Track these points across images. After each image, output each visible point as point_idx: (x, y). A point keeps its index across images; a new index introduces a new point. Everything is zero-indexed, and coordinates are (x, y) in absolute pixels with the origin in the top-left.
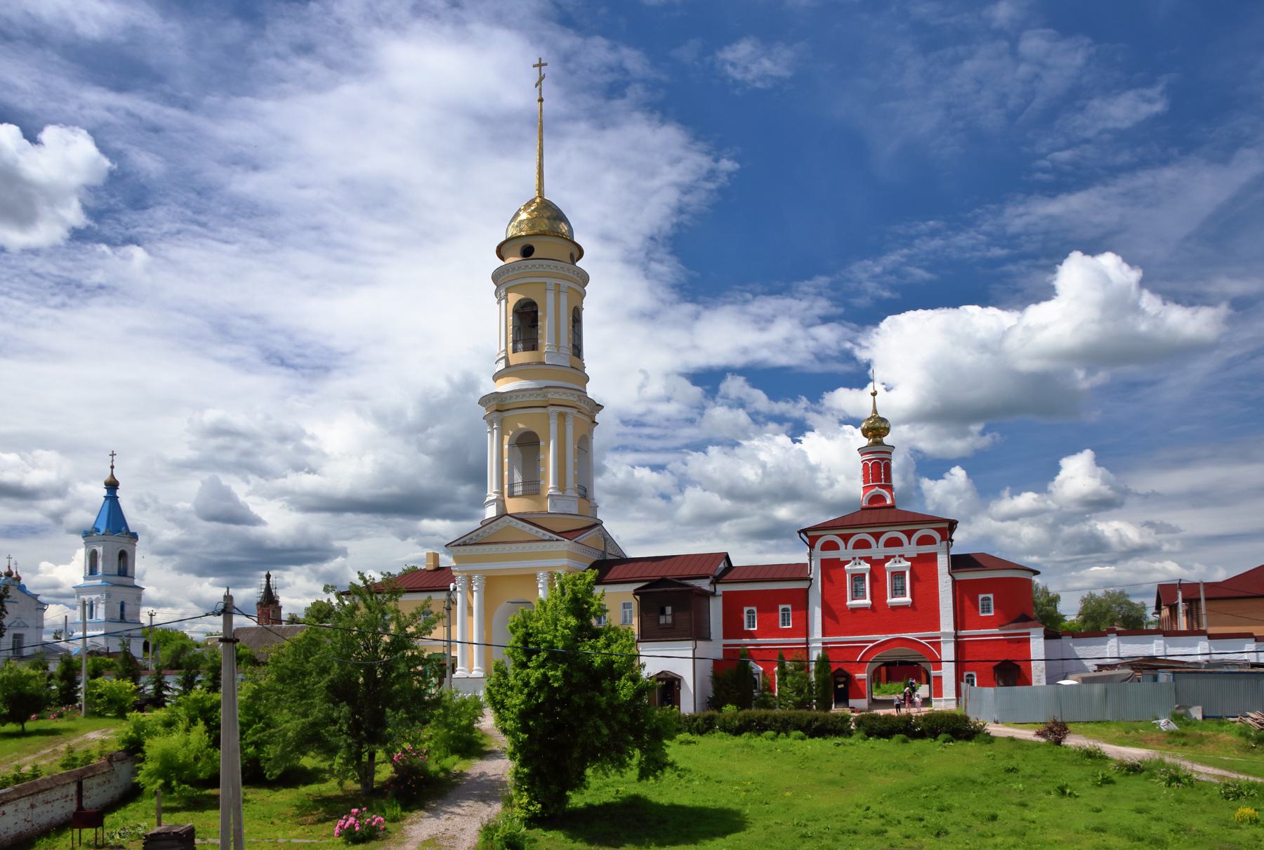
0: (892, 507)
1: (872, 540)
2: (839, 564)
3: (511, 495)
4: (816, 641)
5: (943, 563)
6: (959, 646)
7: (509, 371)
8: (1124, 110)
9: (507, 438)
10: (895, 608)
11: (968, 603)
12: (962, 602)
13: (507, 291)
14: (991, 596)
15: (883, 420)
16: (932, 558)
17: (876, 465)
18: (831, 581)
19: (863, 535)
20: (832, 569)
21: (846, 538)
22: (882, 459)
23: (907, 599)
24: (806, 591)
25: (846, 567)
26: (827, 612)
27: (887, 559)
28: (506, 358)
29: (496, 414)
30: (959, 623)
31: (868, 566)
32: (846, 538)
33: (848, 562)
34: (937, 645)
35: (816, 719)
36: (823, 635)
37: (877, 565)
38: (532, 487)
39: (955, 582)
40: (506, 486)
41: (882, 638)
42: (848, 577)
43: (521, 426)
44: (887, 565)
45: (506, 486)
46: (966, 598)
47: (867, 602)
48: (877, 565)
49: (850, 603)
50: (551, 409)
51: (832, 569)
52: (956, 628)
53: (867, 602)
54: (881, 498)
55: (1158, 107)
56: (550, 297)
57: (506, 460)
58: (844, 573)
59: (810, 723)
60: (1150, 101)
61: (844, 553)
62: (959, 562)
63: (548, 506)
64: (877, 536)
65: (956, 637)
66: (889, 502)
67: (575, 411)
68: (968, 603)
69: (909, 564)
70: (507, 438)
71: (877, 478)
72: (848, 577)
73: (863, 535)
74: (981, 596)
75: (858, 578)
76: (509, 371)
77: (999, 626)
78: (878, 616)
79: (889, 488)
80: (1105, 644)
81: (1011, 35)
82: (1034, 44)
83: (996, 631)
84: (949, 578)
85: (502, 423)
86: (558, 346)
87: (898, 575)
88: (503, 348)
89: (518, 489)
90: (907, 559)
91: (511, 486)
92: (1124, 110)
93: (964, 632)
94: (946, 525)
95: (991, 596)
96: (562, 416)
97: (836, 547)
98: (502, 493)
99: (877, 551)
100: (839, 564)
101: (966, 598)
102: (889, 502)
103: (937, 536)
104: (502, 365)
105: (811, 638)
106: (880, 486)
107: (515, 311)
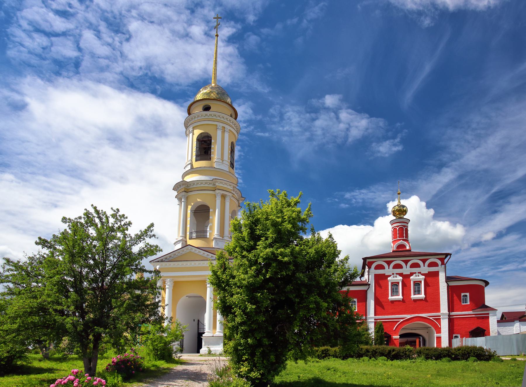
0: (410, 250)
1: (403, 264)
2: (384, 277)
3: (191, 238)
4: (371, 318)
5: (442, 277)
6: (451, 321)
7: (193, 171)
8: (386, 149)
9: (190, 207)
10: (415, 301)
11: (455, 298)
12: (452, 297)
13: (194, 128)
14: (468, 294)
15: (404, 206)
16: (436, 274)
17: (401, 229)
18: (380, 286)
19: (398, 261)
20: (380, 279)
21: (389, 263)
22: (404, 226)
23: (422, 296)
24: (365, 292)
25: (389, 278)
26: (378, 303)
27: (412, 274)
28: (192, 166)
29: (184, 193)
30: (451, 308)
31: (401, 278)
32: (389, 263)
33: (390, 276)
34: (439, 320)
35: (394, 350)
36: (375, 315)
37: (406, 278)
38: (201, 234)
39: (448, 287)
40: (188, 234)
41: (408, 316)
42: (390, 284)
43: (199, 200)
44: (411, 277)
45: (188, 234)
46: (455, 295)
47: (400, 297)
48: (406, 278)
49: (390, 298)
50: (217, 191)
51: (380, 279)
52: (449, 311)
53: (400, 297)
54: (403, 246)
55: (400, 148)
56: (219, 133)
57: (189, 219)
58: (388, 281)
59: (390, 352)
60: (395, 145)
61: (387, 271)
62: (448, 279)
63: (213, 244)
64: (406, 262)
65: (449, 316)
66: (408, 248)
67: (231, 195)
68: (455, 298)
69: (424, 277)
70: (190, 207)
71: (401, 235)
72: (390, 284)
73: (398, 261)
74: (462, 294)
75: (395, 285)
76: (193, 171)
77: (472, 310)
78: (405, 305)
79: (407, 240)
80: (513, 326)
81: (336, 111)
82: (344, 115)
83: (471, 312)
84: (446, 284)
85: (187, 198)
86: (222, 159)
87: (417, 284)
88: (190, 158)
89: (194, 235)
90: (423, 275)
91: (191, 233)
92: (386, 149)
93: (453, 313)
94: (444, 257)
95: (468, 294)
96: (224, 197)
97: (382, 267)
98: (186, 237)
99: (406, 270)
100: (384, 277)
101: (455, 295)
102: (408, 248)
103: (439, 262)
104: (189, 167)
105: (368, 317)
106: (403, 240)
107: (198, 140)
